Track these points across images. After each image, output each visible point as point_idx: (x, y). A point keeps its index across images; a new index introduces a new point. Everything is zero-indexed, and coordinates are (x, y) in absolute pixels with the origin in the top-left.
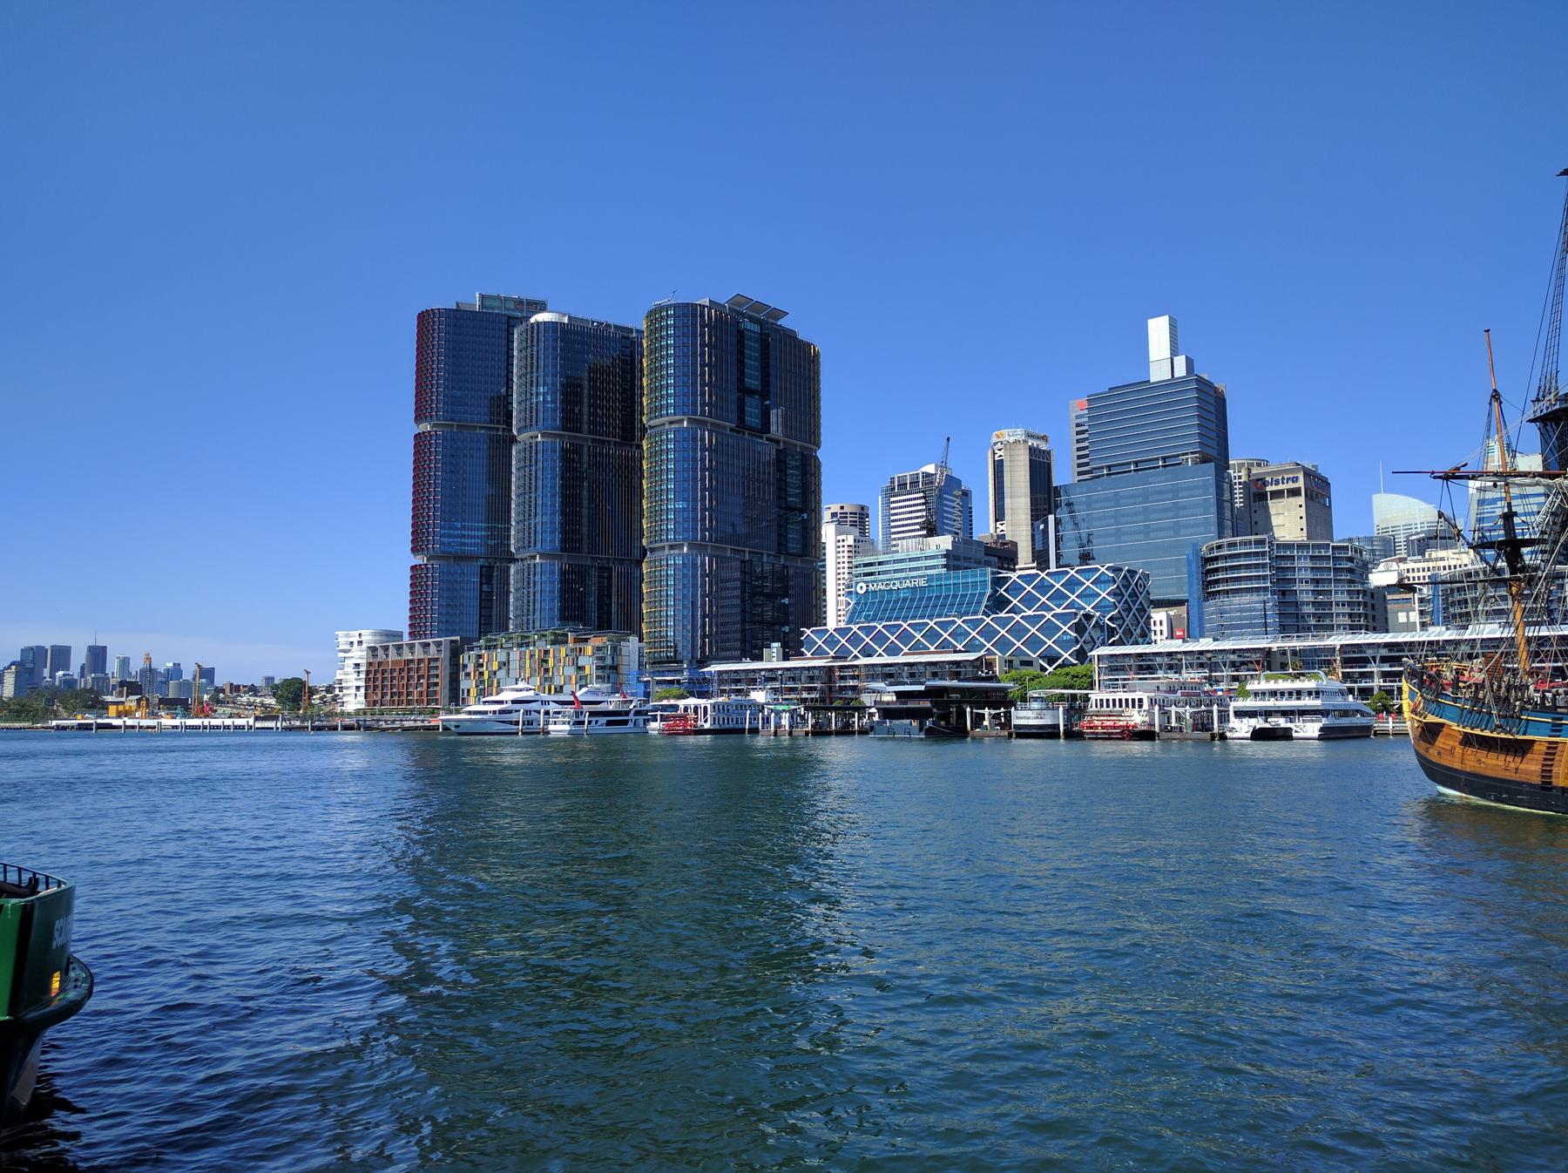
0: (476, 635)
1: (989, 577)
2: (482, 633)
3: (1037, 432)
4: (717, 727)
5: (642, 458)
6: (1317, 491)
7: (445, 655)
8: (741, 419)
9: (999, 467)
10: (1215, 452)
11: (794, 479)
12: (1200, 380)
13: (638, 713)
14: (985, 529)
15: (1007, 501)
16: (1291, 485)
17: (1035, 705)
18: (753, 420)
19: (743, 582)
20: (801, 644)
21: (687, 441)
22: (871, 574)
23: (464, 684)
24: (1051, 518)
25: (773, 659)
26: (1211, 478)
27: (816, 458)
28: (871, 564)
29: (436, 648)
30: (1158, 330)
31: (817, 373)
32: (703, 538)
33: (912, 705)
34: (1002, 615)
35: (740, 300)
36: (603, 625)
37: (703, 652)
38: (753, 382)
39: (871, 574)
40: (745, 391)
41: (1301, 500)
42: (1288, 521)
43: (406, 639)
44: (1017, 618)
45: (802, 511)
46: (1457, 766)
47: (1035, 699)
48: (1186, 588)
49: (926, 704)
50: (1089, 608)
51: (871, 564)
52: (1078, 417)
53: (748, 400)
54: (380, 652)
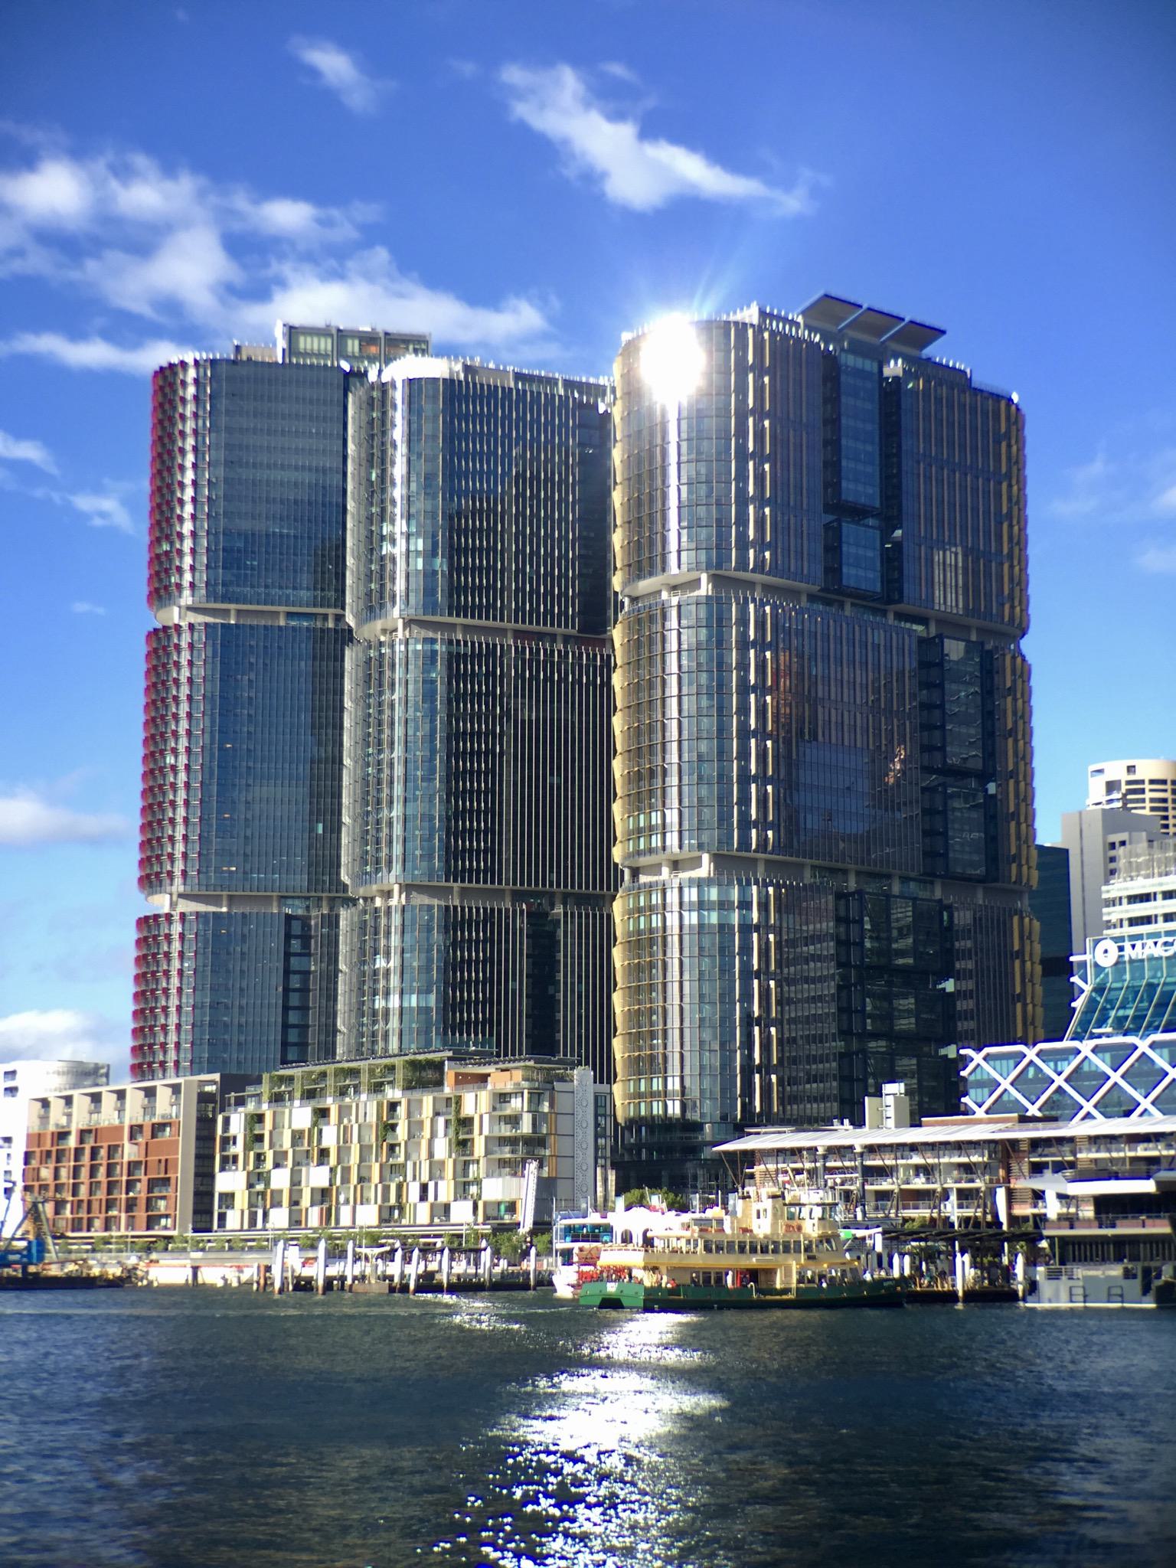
8: (833, 570)
19: (842, 943)
22: (1147, 920)
25: (885, 1118)
28: (1145, 898)
29: (171, 1101)
33: (1126, 1229)
36: (542, 1041)
37: (747, 1107)
39: (1147, 920)
40: (842, 510)
45: (985, 777)
51: (1145, 898)
53: (848, 529)
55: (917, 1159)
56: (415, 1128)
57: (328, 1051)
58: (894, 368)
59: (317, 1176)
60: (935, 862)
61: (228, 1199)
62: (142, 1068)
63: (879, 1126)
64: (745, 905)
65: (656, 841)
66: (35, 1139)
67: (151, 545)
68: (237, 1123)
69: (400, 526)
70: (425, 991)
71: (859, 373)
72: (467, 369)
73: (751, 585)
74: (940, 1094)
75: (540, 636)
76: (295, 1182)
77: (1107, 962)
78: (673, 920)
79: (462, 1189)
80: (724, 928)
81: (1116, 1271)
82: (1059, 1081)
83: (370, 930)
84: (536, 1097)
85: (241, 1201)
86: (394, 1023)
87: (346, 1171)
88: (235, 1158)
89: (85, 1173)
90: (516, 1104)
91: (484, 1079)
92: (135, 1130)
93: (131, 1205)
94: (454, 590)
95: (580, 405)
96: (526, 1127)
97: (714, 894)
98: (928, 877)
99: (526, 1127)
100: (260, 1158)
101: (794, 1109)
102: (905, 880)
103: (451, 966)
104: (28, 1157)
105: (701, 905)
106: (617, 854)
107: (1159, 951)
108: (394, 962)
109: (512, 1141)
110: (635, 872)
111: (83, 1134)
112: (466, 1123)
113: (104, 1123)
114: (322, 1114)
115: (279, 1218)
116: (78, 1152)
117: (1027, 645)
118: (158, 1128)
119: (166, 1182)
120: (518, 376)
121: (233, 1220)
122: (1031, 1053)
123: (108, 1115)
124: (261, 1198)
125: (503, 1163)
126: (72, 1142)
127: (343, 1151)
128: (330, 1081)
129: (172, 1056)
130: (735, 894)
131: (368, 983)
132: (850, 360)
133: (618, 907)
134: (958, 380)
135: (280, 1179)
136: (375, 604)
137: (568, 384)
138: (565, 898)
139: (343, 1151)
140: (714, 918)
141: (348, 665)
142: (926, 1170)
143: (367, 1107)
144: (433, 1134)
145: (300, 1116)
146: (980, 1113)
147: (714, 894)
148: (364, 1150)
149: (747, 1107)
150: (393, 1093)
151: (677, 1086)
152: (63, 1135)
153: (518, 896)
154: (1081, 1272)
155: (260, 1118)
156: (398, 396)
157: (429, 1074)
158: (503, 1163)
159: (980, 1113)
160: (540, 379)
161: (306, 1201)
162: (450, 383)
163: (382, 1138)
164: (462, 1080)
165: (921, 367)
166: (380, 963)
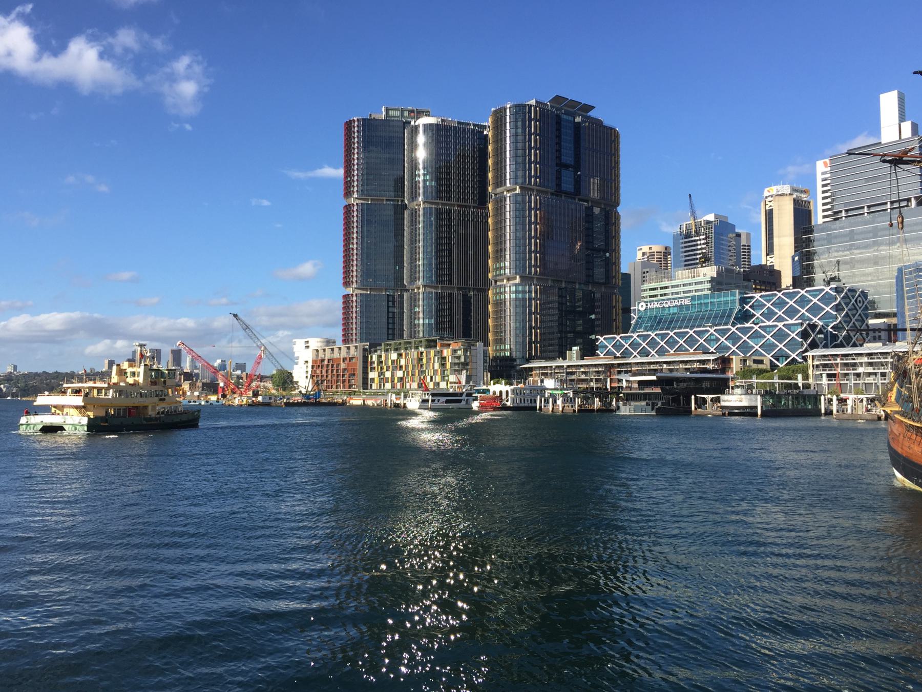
1: (738, 297)
3: (800, 187)
4: (516, 405)
8: (559, 185)
9: (770, 215)
11: (598, 225)
14: (760, 258)
15: (776, 240)
17: (739, 391)
20: (597, 348)
21: (520, 205)
22: (655, 296)
25: (573, 357)
27: (616, 212)
28: (655, 289)
30: (889, 102)
31: (617, 150)
35: (558, 99)
37: (530, 354)
38: (568, 159)
40: (562, 166)
45: (605, 251)
47: (738, 387)
48: (895, 304)
49: (658, 390)
50: (815, 320)
51: (655, 289)
52: (823, 173)
53: (564, 172)
54: (321, 352)
55: (582, 370)
56: (429, 359)
57: (402, 337)
58: (578, 119)
59: (400, 374)
60: (590, 279)
61: (373, 380)
62: (346, 340)
63: (571, 359)
64: (530, 292)
65: (502, 272)
66: (314, 361)
68: (375, 358)
70: (430, 318)
71: (568, 121)
72: (442, 120)
73: (533, 190)
74: (589, 350)
75: (466, 207)
76: (393, 375)
77: (642, 309)
79: (443, 379)
80: (524, 299)
81: (644, 403)
82: (627, 346)
83: (414, 300)
84: (465, 351)
85: (377, 380)
86: (421, 328)
87: (408, 372)
89: (330, 372)
91: (449, 345)
92: (344, 359)
93: (344, 382)
94: (438, 192)
96: (462, 360)
98: (587, 283)
99: (462, 360)
100: (382, 368)
102: (580, 284)
103: (438, 310)
104: (313, 367)
105: (516, 292)
106: (490, 276)
107: (659, 306)
108: (421, 309)
109: (458, 364)
110: (496, 282)
112: (444, 358)
115: (388, 386)
116: (328, 366)
117: (619, 209)
118: (351, 359)
120: (459, 123)
123: (336, 355)
124: (383, 380)
126: (326, 362)
127: (407, 366)
129: (354, 337)
130: (527, 288)
131: (413, 316)
132: (564, 117)
133: (490, 292)
134: (598, 123)
135: (388, 374)
137: (474, 125)
139: (407, 366)
142: (585, 373)
143: (414, 353)
145: (394, 356)
146: (602, 356)
148: (413, 366)
149: (530, 354)
150: (422, 349)
151: (509, 348)
152: (323, 360)
153: (459, 289)
154: (633, 403)
157: (433, 344)
159: (602, 356)
161: (396, 381)
162: (437, 125)
163: (418, 363)
164: (442, 345)
166: (417, 309)
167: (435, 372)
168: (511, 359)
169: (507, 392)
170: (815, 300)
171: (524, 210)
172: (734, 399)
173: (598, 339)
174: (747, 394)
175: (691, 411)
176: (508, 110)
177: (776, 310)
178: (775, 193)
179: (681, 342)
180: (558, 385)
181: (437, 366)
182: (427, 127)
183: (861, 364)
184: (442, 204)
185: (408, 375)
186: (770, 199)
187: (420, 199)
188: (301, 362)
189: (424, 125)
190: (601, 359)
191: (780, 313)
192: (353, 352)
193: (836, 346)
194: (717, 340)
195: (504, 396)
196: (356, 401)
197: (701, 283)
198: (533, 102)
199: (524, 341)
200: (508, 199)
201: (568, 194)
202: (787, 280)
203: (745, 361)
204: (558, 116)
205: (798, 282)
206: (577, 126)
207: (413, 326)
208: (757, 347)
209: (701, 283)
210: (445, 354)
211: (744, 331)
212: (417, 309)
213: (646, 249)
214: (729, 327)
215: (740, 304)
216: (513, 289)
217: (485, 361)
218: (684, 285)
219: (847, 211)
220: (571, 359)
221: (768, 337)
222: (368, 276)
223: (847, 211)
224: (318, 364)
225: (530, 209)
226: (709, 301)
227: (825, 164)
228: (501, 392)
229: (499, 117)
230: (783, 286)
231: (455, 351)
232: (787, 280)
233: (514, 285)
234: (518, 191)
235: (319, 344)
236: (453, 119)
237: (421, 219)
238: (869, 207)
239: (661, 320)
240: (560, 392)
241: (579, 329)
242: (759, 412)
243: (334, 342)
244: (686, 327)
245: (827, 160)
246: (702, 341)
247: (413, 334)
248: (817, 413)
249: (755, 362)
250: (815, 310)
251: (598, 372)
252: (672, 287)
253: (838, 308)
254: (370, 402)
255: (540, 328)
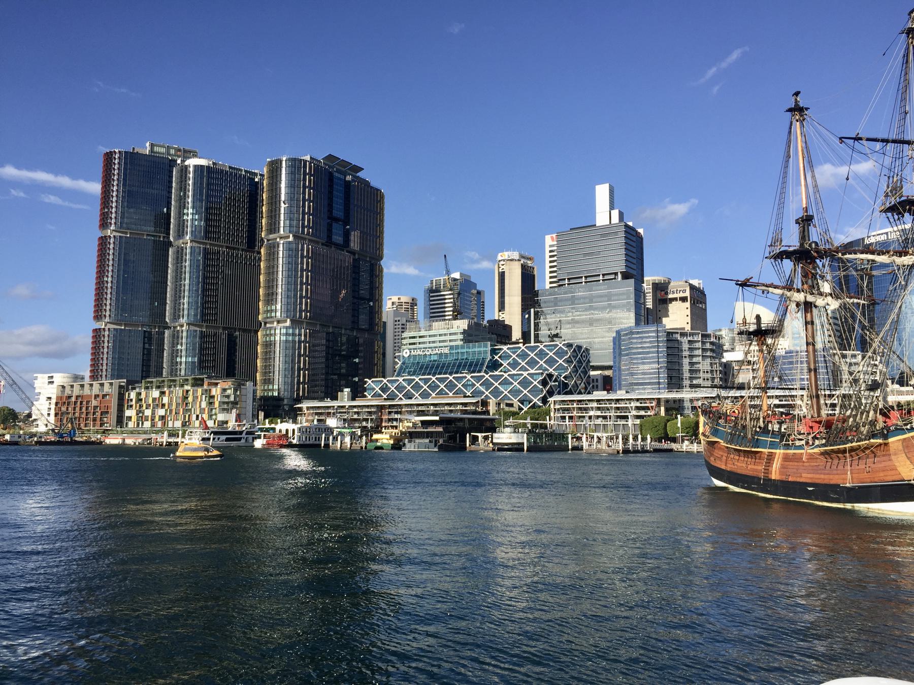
0: (139, 379)
1: (489, 348)
2: (143, 377)
5: (260, 259)
6: (698, 298)
7: (114, 392)
9: (502, 276)
10: (634, 270)
11: (364, 276)
12: (627, 226)
13: (248, 433)
14: (492, 313)
15: (507, 298)
16: (682, 295)
17: (508, 430)
18: (338, 239)
19: (328, 347)
20: (365, 390)
21: (292, 251)
22: (414, 344)
23: (128, 413)
24: (532, 310)
25: (345, 397)
26: (632, 289)
27: (380, 265)
28: (414, 337)
29: (110, 387)
32: (301, 316)
34: (497, 373)
35: (330, 158)
36: (230, 373)
38: (338, 212)
39: (414, 344)
40: (332, 219)
41: (688, 304)
42: (678, 317)
43: (87, 380)
44: (506, 375)
45: (370, 300)
46: (723, 467)
47: (507, 426)
49: (440, 429)
50: (551, 370)
51: (414, 337)
52: (550, 246)
53: (334, 225)
55: (355, 410)
56: (195, 398)
57: (161, 375)
58: (349, 178)
59: (161, 412)
60: (355, 325)
61: (130, 418)
62: (95, 376)
63: (342, 400)
64: (300, 335)
65: (273, 314)
66: (59, 398)
67: (101, 209)
68: (133, 395)
69: (190, 211)
70: (193, 356)
71: (340, 179)
72: (214, 163)
73: (305, 239)
74: (358, 392)
75: (234, 249)
76: (153, 413)
77: (406, 356)
78: (277, 338)
79: (210, 417)
80: (294, 342)
81: (427, 441)
82: (393, 388)
83: (176, 337)
84: (235, 390)
85: (134, 419)
86: (183, 366)
87: (171, 411)
88: (131, 406)
89: (78, 409)
90: (229, 392)
91: (217, 384)
92: (96, 396)
93: (95, 420)
94: (207, 232)
95: (249, 178)
96: (232, 399)
97: (291, 331)
98: (352, 329)
99: (232, 399)
100: (141, 406)
101: (312, 395)
102: (346, 329)
103: (201, 349)
104: (57, 404)
105: (287, 334)
106: (260, 318)
107: (421, 353)
108: (184, 347)
109: (227, 403)
110: (265, 323)
111: (77, 397)
112: (213, 397)
113: (85, 393)
114: (163, 393)
115: (147, 424)
116: (75, 403)
117: (382, 262)
118: (104, 396)
119: (107, 412)
120: (230, 167)
121: (131, 425)
122: (385, 381)
123: (87, 391)
124: (141, 418)
125: (224, 409)
126: (73, 399)
127: (170, 404)
128: (166, 383)
129: (104, 373)
130: (297, 332)
131: (174, 354)
132: (336, 174)
133: (259, 334)
134: (367, 183)
135: (148, 413)
136: (180, 234)
137: (246, 171)
138: (239, 330)
139: (170, 404)
140: (290, 338)
141: (170, 253)
142: (358, 413)
143: (179, 392)
144: (201, 400)
145: (156, 393)
146: (369, 397)
147: (291, 331)
148: (178, 404)
149: (298, 394)
150: (186, 388)
151: (277, 387)
152: (70, 397)
153: (224, 329)
154: (417, 441)
155: (140, 394)
156: (191, 169)
157: (199, 382)
158: (224, 409)
159: (369, 397)
160: (237, 169)
161: (157, 419)
162: (208, 167)
163: (183, 401)
164: (210, 384)
165: (356, 178)
166: (179, 347)
167: (202, 411)
168: (279, 399)
169: (294, 430)
170: (551, 354)
171: (296, 256)
172: (505, 436)
173: (366, 382)
174: (515, 432)
175: (465, 448)
176: (284, 163)
177: (520, 361)
178: (506, 258)
179: (442, 386)
180: (341, 424)
181: (204, 405)
182: (198, 168)
183: (592, 408)
184: (211, 244)
185: (171, 413)
186: (502, 263)
187: (188, 238)
188: (43, 398)
189: (195, 166)
190: (369, 400)
191: (523, 364)
192: (107, 389)
193: (566, 393)
194: (473, 385)
195: (290, 434)
196: (113, 440)
197: (455, 334)
198: (308, 158)
199: (293, 381)
200: (281, 246)
201: (337, 246)
202: (516, 334)
203: (499, 404)
204: (331, 174)
205: (526, 337)
206: (347, 184)
207: (174, 364)
208: (506, 392)
209: (455, 334)
210: (213, 392)
211: (496, 378)
212: (179, 347)
213: (395, 299)
214: (482, 374)
215: (491, 355)
216: (284, 331)
217: (254, 400)
218: (440, 335)
219: (569, 279)
220: (342, 400)
221: (515, 384)
222: (123, 309)
223: (569, 279)
224: (63, 403)
225: (302, 257)
226: (465, 350)
227: (552, 238)
228: (287, 431)
229: (275, 168)
230: (514, 339)
231: (224, 390)
232: (516, 334)
233: (284, 327)
234: (291, 239)
235: (66, 380)
236: (225, 163)
237: (188, 257)
238: (586, 277)
239: (422, 366)
240: (348, 431)
241: (343, 371)
242: (525, 448)
243: (83, 378)
244: (429, 374)
245: (554, 235)
246: (460, 386)
247: (173, 371)
248: (566, 449)
249: (507, 405)
250: (551, 362)
251: (370, 413)
252: (430, 336)
253: (569, 361)
254: (130, 441)
255: (308, 370)
